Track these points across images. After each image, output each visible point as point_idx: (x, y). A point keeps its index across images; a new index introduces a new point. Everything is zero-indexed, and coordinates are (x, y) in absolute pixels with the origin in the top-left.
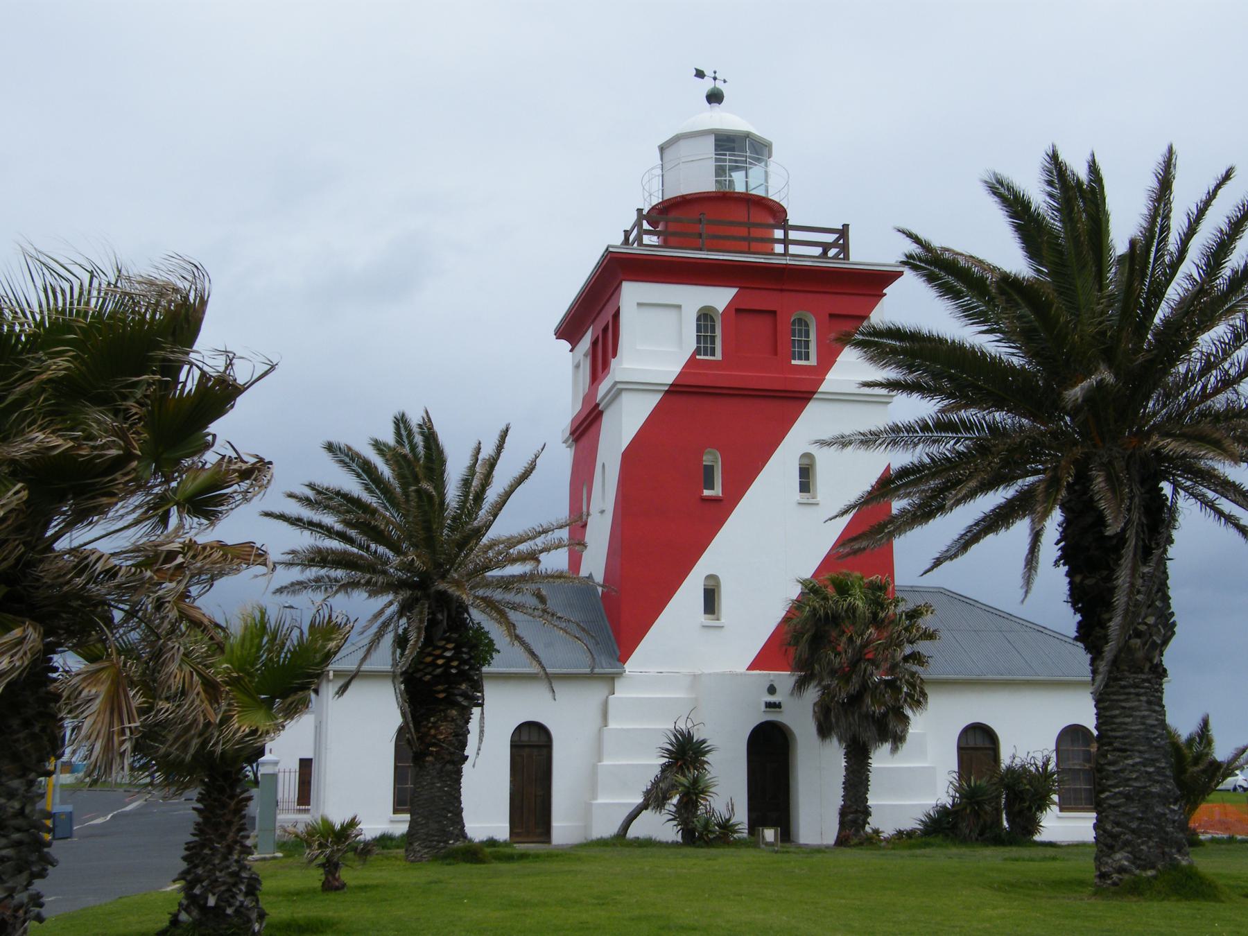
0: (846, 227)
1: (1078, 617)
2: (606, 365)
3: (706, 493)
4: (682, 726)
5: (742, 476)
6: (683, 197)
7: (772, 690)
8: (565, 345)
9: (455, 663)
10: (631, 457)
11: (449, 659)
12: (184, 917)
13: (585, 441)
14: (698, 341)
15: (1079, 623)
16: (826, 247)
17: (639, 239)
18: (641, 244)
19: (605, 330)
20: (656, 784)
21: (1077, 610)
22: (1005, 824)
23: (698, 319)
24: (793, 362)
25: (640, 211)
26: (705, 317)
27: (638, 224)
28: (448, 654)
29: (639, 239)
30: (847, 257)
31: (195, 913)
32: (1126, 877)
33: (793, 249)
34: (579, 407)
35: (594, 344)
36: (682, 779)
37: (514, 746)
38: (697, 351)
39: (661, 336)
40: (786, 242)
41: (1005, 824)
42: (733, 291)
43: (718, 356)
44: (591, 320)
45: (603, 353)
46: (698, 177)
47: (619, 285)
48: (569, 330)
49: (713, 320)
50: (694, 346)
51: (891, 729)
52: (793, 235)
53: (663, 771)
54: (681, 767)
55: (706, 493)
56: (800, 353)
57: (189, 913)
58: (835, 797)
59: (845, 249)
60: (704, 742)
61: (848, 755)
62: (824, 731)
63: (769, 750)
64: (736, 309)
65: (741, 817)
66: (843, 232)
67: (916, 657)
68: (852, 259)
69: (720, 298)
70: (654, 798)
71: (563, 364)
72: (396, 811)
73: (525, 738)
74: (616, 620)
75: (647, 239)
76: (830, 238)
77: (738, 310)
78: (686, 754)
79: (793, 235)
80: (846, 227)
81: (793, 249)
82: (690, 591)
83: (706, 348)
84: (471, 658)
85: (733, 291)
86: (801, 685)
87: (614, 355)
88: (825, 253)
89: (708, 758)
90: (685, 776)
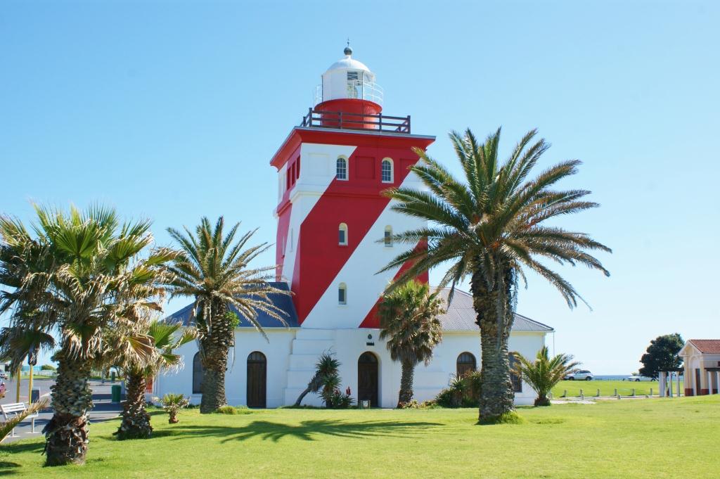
0: (409, 117)
1: (478, 314)
2: (294, 182)
3: (341, 244)
4: (326, 353)
5: (357, 236)
6: (186, 308)
7: (370, 337)
8: (275, 169)
9: (222, 328)
10: (305, 227)
11: (219, 326)
12: (123, 429)
13: (283, 216)
14: (338, 172)
15: (478, 316)
16: (400, 126)
17: (310, 122)
18: (311, 125)
19: (294, 165)
20: (314, 380)
21: (476, 311)
22: (121, 401)
23: (338, 161)
24: (383, 182)
25: (311, 109)
26: (340, 162)
27: (310, 115)
28: (219, 324)
29: (310, 122)
30: (409, 132)
31: (127, 428)
32: (489, 416)
33: (384, 127)
34: (281, 200)
35: (289, 171)
36: (325, 378)
37: (249, 362)
38: (337, 176)
39: (323, 164)
40: (380, 124)
41: (121, 401)
42: (356, 147)
43: (347, 179)
44: (288, 160)
45: (293, 176)
46: (343, 93)
47: (300, 145)
48: (277, 162)
49: (344, 161)
50: (335, 174)
51: (423, 353)
52: (384, 121)
53: (317, 375)
54: (325, 372)
55: (341, 244)
56: (386, 177)
57: (125, 428)
58: (398, 387)
59: (408, 127)
60: (335, 361)
61: (403, 367)
62: (394, 357)
63: (368, 365)
64: (354, 157)
65: (354, 395)
66: (408, 119)
67: (436, 322)
68: (411, 133)
69: (347, 151)
70: (313, 386)
71: (277, 177)
72: (194, 392)
73: (254, 359)
74: (294, 304)
75: (314, 123)
76: (401, 122)
77: (356, 157)
78: (327, 369)
79: (384, 121)
80: (409, 117)
81: (384, 127)
82: (331, 292)
83: (341, 175)
84: (229, 325)
85: (356, 147)
86: (383, 335)
87: (298, 178)
88: (400, 128)
89: (338, 368)
90: (326, 376)
